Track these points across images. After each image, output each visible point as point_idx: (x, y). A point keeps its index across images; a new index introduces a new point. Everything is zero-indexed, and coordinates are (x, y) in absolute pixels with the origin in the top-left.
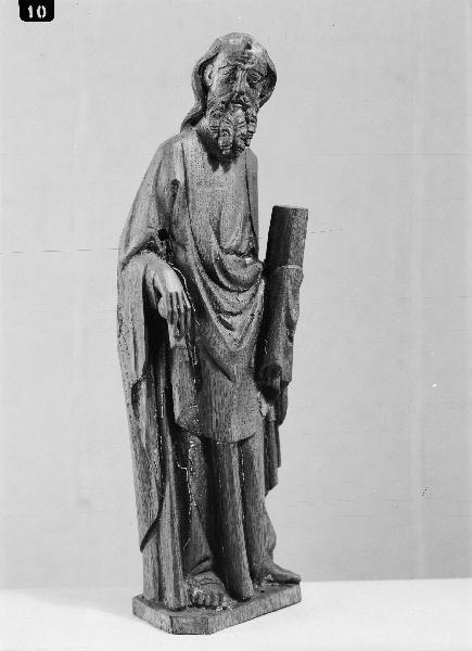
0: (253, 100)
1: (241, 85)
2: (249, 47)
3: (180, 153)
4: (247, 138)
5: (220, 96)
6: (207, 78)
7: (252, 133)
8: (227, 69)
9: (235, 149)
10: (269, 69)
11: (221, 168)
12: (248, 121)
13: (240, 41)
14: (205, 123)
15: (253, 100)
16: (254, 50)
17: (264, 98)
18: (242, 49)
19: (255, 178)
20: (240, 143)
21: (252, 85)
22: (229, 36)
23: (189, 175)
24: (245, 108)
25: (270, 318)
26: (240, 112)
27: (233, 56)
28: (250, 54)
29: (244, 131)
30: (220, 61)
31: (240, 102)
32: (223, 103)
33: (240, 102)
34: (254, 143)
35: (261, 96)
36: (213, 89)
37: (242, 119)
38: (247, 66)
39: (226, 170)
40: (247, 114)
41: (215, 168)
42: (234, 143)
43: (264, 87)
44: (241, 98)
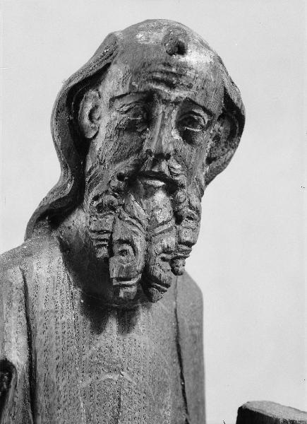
0: (189, 171)
1: (167, 136)
2: (181, 50)
3: (18, 295)
4: (175, 258)
5: (116, 161)
6: (86, 121)
7: (190, 244)
8: (129, 101)
9: (149, 285)
10: (227, 97)
11: (112, 325)
12: (178, 218)
13: (159, 36)
14: (80, 220)
15: (189, 171)
16: (193, 58)
17: (216, 164)
18: (162, 55)
19: (198, 339)
20: (161, 270)
21: (188, 137)
22: (136, 29)
23: (37, 345)
24: (172, 187)
25: (35, 380)
26: (160, 197)
27: (141, 70)
28: (184, 66)
29: (170, 241)
30: (112, 85)
31: (160, 176)
32: (120, 177)
33: (160, 176)
34: (192, 265)
35: (209, 160)
36: (99, 144)
37: (164, 214)
38: (176, 94)
39: (127, 324)
40: (175, 203)
41: (98, 327)
42: (146, 271)
43: (217, 138)
44: (164, 166)
